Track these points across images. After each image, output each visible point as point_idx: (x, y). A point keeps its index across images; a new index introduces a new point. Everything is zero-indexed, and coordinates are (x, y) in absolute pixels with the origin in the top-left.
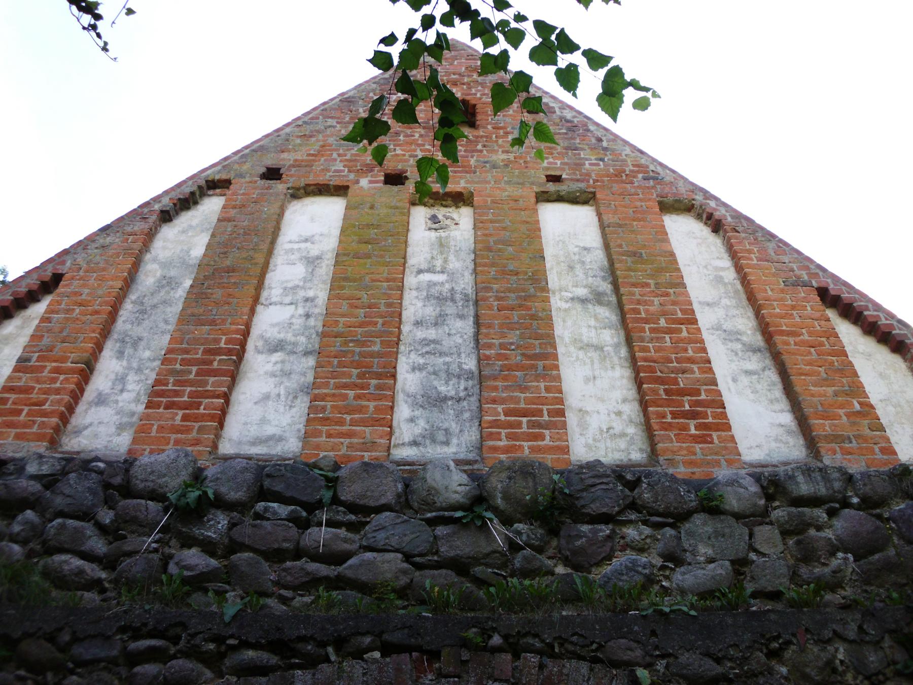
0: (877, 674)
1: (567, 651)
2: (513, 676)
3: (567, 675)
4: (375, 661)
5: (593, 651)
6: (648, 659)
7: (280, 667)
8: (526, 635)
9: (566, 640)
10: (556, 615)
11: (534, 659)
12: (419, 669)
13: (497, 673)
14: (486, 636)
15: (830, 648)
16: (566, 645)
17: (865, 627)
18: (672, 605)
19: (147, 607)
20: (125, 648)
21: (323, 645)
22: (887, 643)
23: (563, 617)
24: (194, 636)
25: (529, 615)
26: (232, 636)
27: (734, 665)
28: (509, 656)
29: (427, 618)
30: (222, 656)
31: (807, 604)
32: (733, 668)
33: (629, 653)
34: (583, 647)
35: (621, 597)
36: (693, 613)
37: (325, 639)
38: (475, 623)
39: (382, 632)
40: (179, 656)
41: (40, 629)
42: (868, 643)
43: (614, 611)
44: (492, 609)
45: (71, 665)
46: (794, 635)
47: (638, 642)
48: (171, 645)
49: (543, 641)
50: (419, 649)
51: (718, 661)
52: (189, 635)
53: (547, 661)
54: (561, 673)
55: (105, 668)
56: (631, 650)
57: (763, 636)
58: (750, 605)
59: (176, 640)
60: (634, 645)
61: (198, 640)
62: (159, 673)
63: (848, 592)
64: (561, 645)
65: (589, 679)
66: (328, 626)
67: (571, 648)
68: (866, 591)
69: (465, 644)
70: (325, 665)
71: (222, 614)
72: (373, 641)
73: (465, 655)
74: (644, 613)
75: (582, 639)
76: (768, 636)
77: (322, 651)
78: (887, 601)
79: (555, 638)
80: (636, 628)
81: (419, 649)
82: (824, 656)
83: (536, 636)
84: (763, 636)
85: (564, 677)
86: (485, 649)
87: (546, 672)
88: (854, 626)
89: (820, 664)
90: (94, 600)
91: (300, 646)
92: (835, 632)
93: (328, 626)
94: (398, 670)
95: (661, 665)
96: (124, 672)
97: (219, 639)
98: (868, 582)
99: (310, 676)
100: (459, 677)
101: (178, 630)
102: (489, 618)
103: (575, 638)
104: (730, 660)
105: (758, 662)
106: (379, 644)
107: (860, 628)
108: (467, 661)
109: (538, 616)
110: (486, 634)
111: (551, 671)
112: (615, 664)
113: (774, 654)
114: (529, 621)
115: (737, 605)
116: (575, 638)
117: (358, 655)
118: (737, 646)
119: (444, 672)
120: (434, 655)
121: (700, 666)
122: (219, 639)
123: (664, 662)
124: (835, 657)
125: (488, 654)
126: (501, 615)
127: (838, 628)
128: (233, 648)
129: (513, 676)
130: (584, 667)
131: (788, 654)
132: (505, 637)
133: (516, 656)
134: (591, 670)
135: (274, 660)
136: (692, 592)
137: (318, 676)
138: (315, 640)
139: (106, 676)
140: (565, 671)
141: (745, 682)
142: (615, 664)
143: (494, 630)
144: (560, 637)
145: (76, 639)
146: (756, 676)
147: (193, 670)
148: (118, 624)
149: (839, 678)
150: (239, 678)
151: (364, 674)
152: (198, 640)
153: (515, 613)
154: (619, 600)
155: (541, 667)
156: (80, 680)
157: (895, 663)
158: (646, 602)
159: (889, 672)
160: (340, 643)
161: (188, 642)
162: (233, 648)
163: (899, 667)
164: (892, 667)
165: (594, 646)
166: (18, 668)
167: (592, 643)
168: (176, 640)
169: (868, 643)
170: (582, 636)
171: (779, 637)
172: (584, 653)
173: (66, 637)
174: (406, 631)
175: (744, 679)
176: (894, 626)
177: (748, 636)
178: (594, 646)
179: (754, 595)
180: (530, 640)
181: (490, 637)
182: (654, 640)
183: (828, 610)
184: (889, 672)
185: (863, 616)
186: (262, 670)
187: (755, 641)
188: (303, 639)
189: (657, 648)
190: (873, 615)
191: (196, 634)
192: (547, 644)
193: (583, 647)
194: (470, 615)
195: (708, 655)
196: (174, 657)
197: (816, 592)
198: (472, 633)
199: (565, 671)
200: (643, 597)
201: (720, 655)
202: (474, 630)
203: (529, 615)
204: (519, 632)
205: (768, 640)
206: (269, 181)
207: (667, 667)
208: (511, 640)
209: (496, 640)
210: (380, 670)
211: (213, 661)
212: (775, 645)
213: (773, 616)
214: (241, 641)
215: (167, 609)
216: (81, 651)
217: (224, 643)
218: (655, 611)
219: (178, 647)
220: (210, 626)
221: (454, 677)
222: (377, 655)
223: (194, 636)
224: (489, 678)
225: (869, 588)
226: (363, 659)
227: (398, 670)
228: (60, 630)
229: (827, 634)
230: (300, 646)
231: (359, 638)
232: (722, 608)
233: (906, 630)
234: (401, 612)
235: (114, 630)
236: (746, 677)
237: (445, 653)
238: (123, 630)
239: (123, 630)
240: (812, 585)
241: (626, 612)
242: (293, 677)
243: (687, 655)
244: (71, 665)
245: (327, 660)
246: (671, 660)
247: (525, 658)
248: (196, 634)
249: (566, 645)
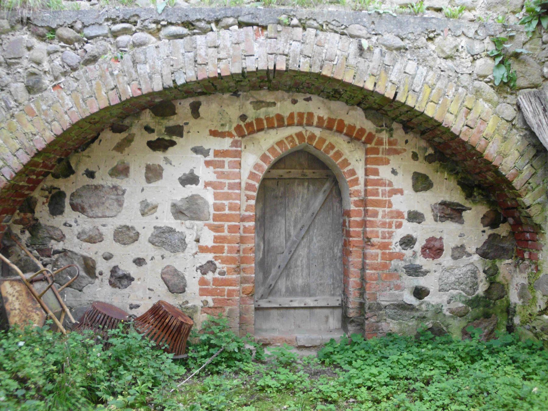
0: (477, 55)
1: (330, 29)
2: (302, 39)
3: (329, 40)
4: (235, 31)
5: (342, 29)
6: (369, 35)
7: (189, 34)
8: (309, 19)
9: (329, 23)
10: (325, 10)
11: (313, 31)
12: (257, 34)
13: (295, 38)
14: (290, 19)
15: (459, 40)
16: (330, 26)
17: (478, 32)
18: (385, 9)
19: (117, 8)
20: (110, 29)
21: (209, 23)
22: (488, 40)
23: (329, 12)
24: (143, 21)
25: (312, 10)
26: (163, 20)
27: (410, 42)
28: (301, 29)
29: (260, 9)
30: (159, 30)
31: (454, 16)
32: (409, 44)
33: (360, 31)
34: (337, 27)
35: (359, 3)
36: (394, 15)
37: (210, 20)
38: (285, 12)
39: (239, 16)
40: (138, 31)
41: (65, 22)
42: (478, 39)
43: (355, 10)
44: (293, 5)
45: (86, 39)
46: (442, 31)
47: (365, 26)
48: (133, 26)
49: (318, 23)
50: (257, 25)
51: (402, 39)
52: (142, 21)
53: (319, 33)
54: (325, 39)
55: (103, 39)
56: (361, 30)
57: (427, 30)
58: (424, 13)
59: (135, 23)
60: (362, 28)
61: (146, 23)
62: (130, 40)
63: (477, 13)
64: (327, 25)
65: (339, 42)
66: (211, 14)
67: (331, 27)
68: (487, 13)
69: (279, 23)
70: (211, 33)
71: (157, 10)
72: (234, 21)
73: (280, 28)
74: (370, 12)
75: (337, 23)
76: (429, 30)
77: (209, 26)
78: (496, 20)
79: (324, 22)
80: (365, 20)
81: (257, 25)
82: (455, 43)
83: (315, 20)
84: (427, 30)
85: (327, 41)
86: (289, 25)
87: (318, 38)
88: (473, 31)
89: (452, 46)
90: (87, 6)
91: (198, 24)
92: (463, 32)
93: (211, 14)
94: (247, 35)
95: (374, 38)
96: (112, 40)
97: (157, 22)
98: (489, 9)
99: (204, 38)
100: (276, 38)
101: (135, 18)
102: (292, 10)
103: (334, 23)
104: (409, 39)
105: (422, 42)
106: (237, 22)
107: (476, 32)
108: (280, 31)
109: (316, 10)
110: (290, 18)
111: (321, 38)
112: (352, 36)
113: (430, 39)
114: (312, 13)
115: (418, 13)
116: (334, 23)
117: (227, 27)
118: (413, 33)
119: (269, 36)
120: (265, 28)
121: (393, 41)
122: (157, 22)
123: (376, 37)
124: (459, 44)
125: (291, 28)
126: (297, 8)
127: (465, 31)
128: (164, 26)
129: (302, 39)
130: (337, 36)
131: (437, 40)
132: (300, 20)
133: (304, 29)
134: (340, 38)
135: (185, 31)
136: (397, 3)
137: (208, 38)
138: (205, 20)
139: (103, 42)
140: (328, 38)
141: (414, 51)
142: (352, 36)
143: (294, 16)
144: (327, 21)
145: (84, 26)
146: (419, 48)
147: (146, 38)
148: (104, 17)
149: (459, 54)
150: (169, 40)
151: (230, 37)
152: (146, 23)
153: (305, 8)
154: (358, 4)
155: (316, 35)
156: (92, 46)
157: (487, 51)
158: (372, 6)
159: (483, 55)
160: (217, 22)
161: (142, 24)
162: (164, 26)
163: (489, 53)
164: (485, 52)
165: (343, 27)
166: (59, 42)
167: (342, 25)
168: (135, 23)
169: (478, 39)
170: (337, 21)
171: (435, 31)
172: (337, 29)
173: (79, 26)
174: (250, 15)
175: (413, 49)
176: (493, 33)
177: (419, 30)
178: (343, 27)
179: (428, 9)
180: (312, 22)
181: (292, 19)
182: (373, 26)
183: (463, 21)
184: (483, 55)
185: (479, 26)
186: (180, 36)
187: (422, 32)
188: (199, 20)
189: (374, 30)
190: (485, 26)
191: (145, 20)
192: (320, 25)
193: (337, 27)
194: (282, 8)
195: (398, 36)
196: (135, 32)
197: (460, 11)
198: (283, 18)
199: (328, 38)
200: (371, 4)
201: (404, 37)
202: (284, 16)
203: (312, 10)
204: (306, 18)
205: (429, 32)
206: (192, 222)
207: (377, 40)
208: (302, 22)
209: (295, 21)
210: (238, 35)
211: (155, 33)
212: (432, 35)
213: (434, 21)
214: (168, 22)
215: (127, 8)
216: (88, 32)
217: (159, 23)
218: (375, 12)
219: (137, 27)
220: (151, 16)
221: (274, 38)
222: (236, 27)
223: (143, 21)
224: (291, 39)
225: (488, 12)
226: (229, 29)
227: (247, 35)
228: (76, 22)
229: (459, 32)
230: (198, 24)
231: (227, 19)
232: (410, 13)
233: (498, 36)
234: (247, 6)
235: (103, 20)
236: (415, 48)
237: (269, 27)
238: (107, 20)
239: (107, 20)
240: (459, 7)
241: (361, 10)
242: (196, 39)
243: (388, 35)
244: (86, 39)
245: (212, 30)
246: (380, 37)
247: (309, 31)
248: (145, 20)
249: (330, 26)
